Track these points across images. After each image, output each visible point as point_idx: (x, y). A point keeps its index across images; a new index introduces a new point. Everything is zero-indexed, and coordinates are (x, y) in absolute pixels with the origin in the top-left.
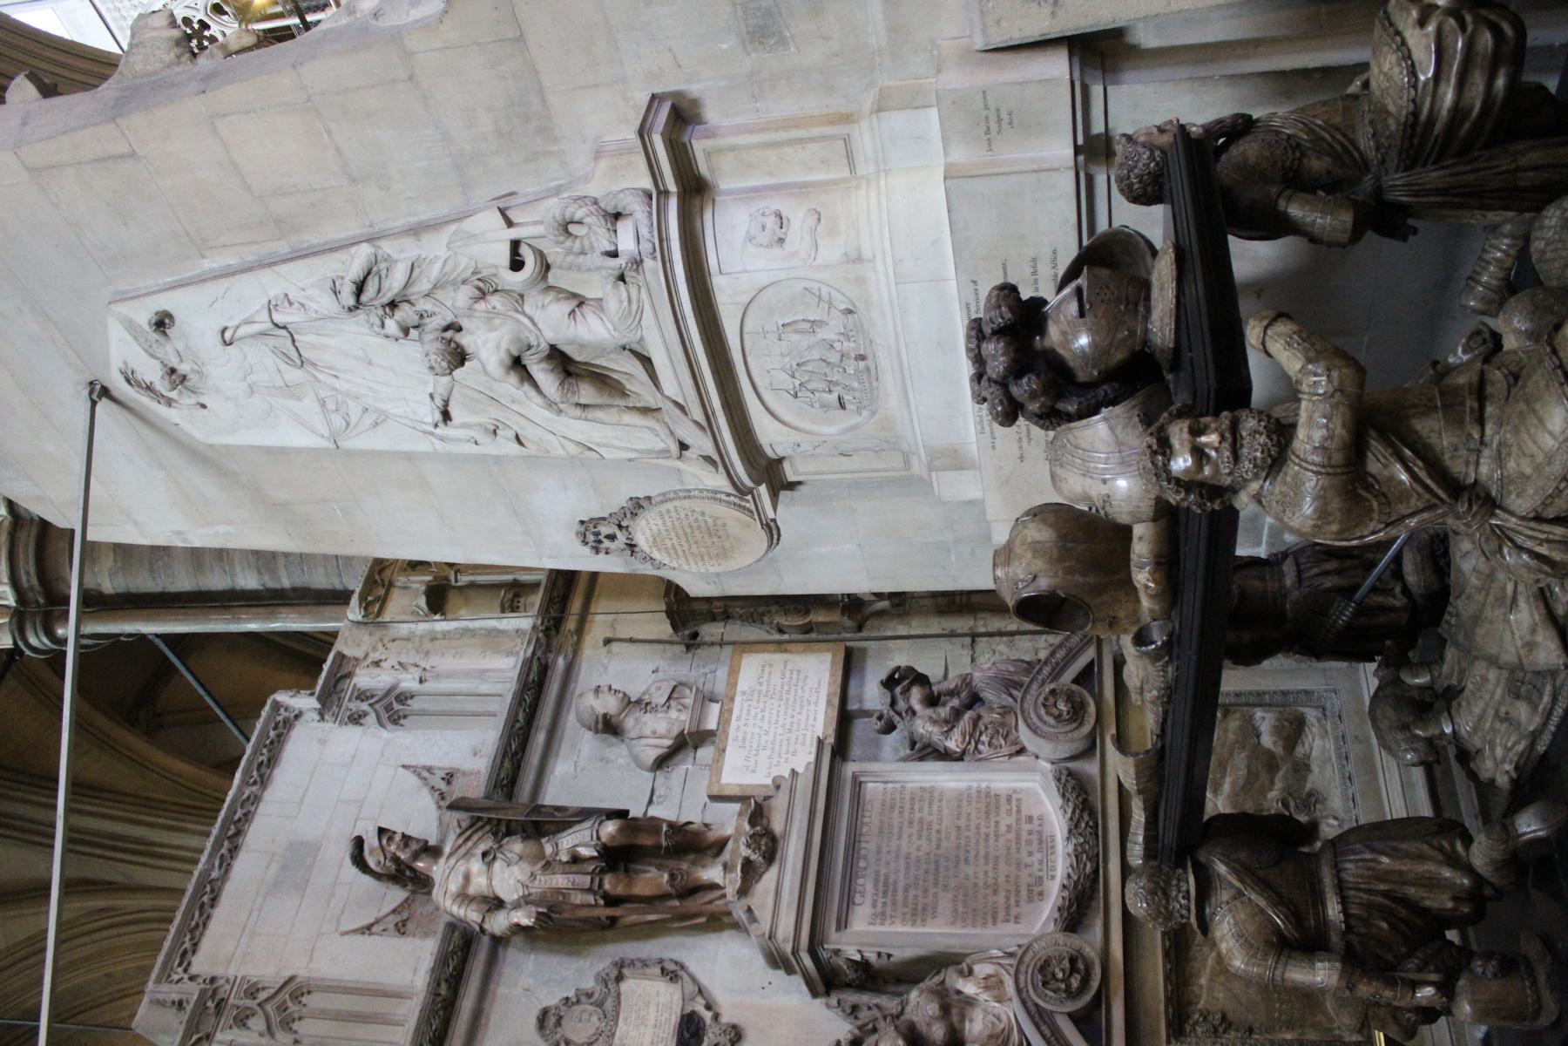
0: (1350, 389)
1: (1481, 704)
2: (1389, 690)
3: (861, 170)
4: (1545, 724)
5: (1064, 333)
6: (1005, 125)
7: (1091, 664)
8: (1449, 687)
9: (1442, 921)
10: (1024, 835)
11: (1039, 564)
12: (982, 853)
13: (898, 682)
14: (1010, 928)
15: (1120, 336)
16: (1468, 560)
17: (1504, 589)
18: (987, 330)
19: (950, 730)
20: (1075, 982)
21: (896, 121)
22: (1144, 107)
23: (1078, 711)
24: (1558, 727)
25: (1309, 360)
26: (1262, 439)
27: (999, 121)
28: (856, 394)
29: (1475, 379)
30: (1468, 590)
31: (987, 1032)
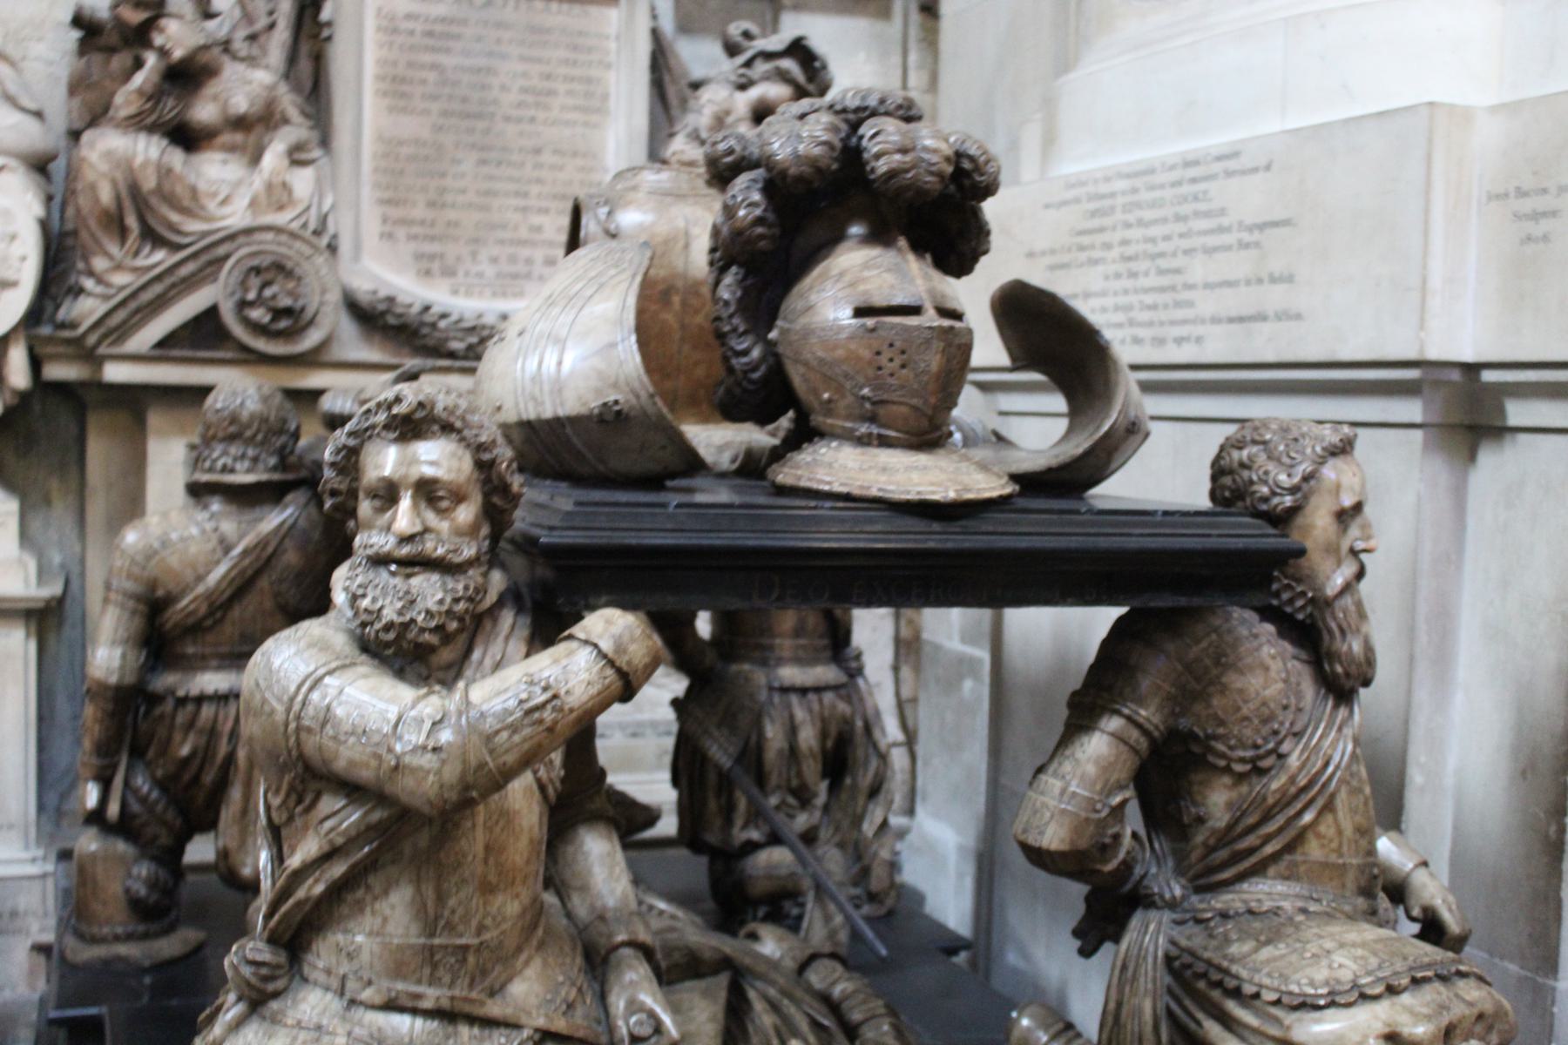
10: (525, 252)
12: (498, 186)
20: (257, 314)
27: (1536, 216)
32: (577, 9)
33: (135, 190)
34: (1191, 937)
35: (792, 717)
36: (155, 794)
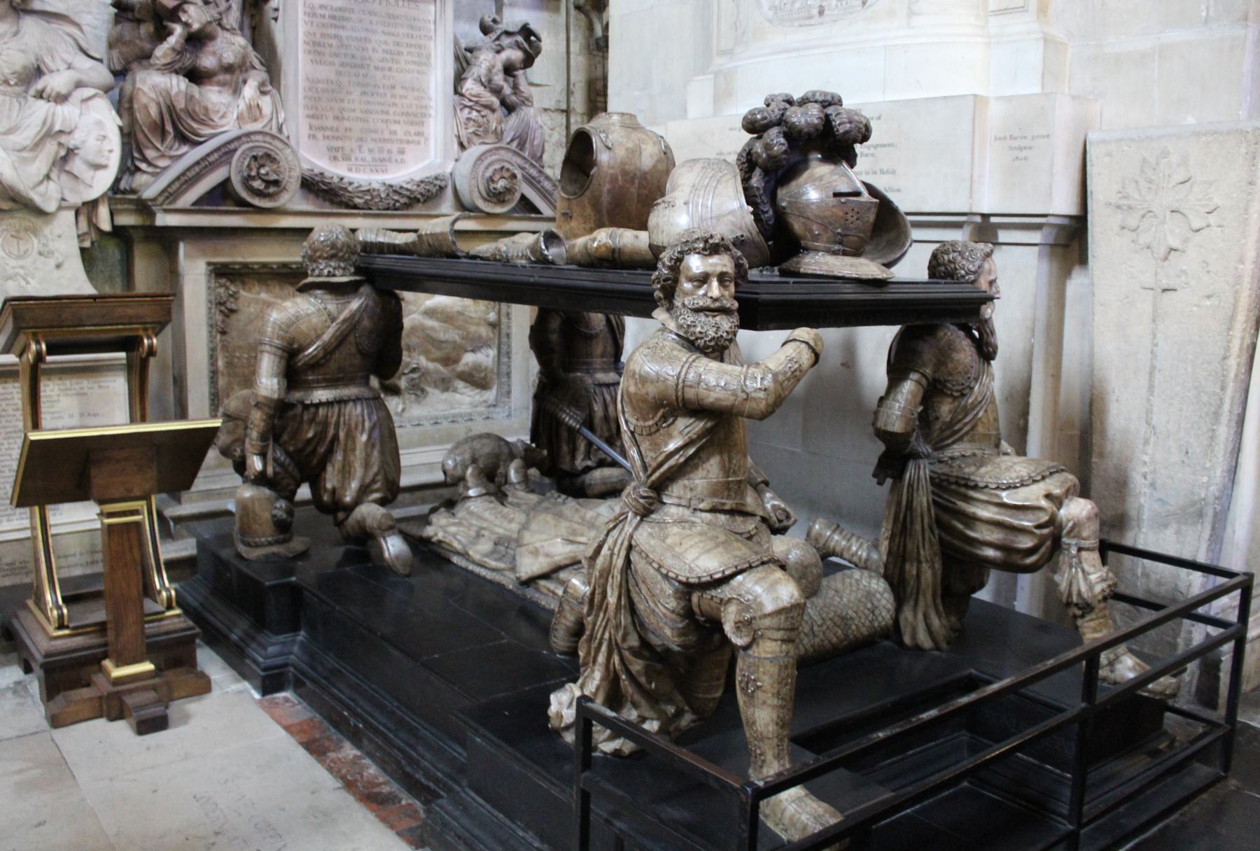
0: (748, 407)
1: (491, 518)
2: (506, 450)
3: (993, 21)
4: (474, 562)
5: (821, 178)
6: (1017, 153)
7: (537, 211)
8: (505, 495)
9: (316, 483)
10: (387, 146)
11: (620, 153)
13: (527, 39)
14: (304, 131)
15: (815, 227)
16: (605, 510)
17: (582, 535)
18: (830, 110)
19: (482, 84)
20: (257, 184)
21: (1034, 55)
22: (1015, 283)
23: (498, 197)
24: (472, 572)
25: (775, 375)
26: (711, 333)
27: (1021, 149)
28: (788, 6)
29: (749, 509)
30: (583, 510)
31: (210, 106)
32: (413, 5)
33: (171, 109)
34: (940, 469)
35: (604, 399)
36: (288, 461)
